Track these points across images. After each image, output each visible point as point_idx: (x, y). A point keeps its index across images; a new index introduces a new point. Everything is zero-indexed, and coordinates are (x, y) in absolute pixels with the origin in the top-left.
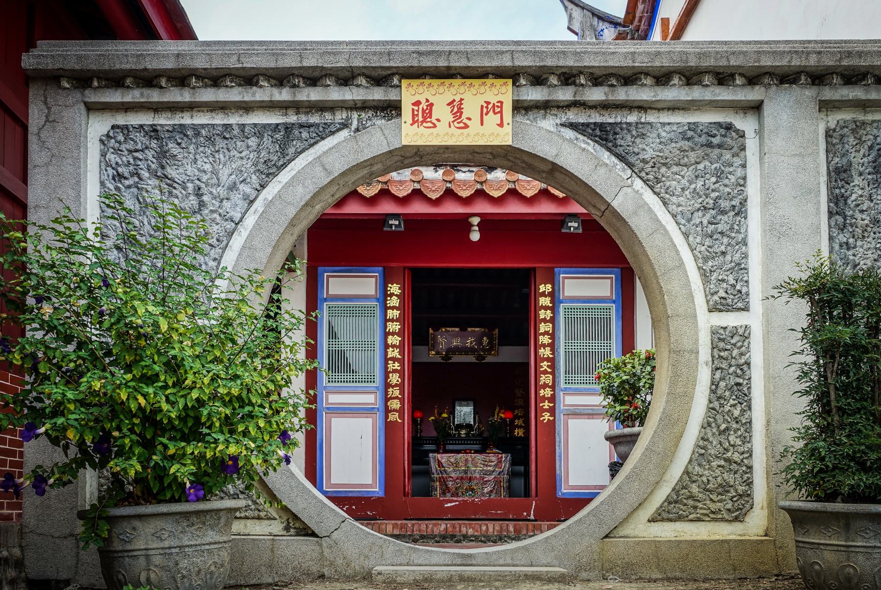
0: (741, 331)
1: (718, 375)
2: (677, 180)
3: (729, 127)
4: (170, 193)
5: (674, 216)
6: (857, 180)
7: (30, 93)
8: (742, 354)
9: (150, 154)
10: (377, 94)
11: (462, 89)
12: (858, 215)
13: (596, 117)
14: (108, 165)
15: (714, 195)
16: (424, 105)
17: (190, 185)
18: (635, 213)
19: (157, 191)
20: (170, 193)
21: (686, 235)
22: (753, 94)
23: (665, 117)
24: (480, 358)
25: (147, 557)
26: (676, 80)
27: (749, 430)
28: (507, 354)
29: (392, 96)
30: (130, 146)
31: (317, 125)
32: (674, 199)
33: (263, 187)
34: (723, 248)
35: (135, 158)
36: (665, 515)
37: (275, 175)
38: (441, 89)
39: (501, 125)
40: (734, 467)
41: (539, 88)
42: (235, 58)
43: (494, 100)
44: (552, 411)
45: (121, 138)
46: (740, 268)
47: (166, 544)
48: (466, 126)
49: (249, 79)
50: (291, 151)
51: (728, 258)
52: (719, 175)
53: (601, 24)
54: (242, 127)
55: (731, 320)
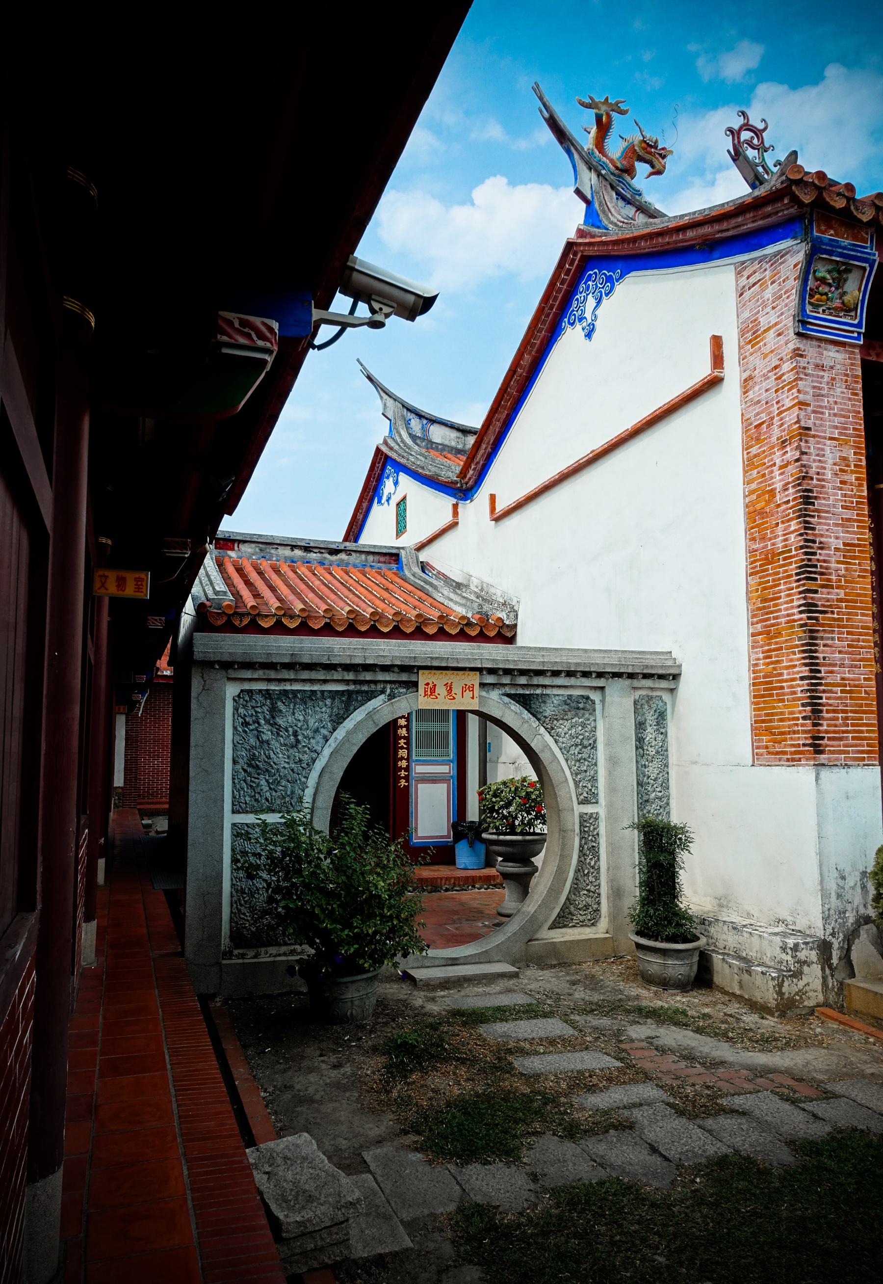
0: (594, 816)
1: (583, 842)
2: (563, 727)
3: (588, 698)
4: (278, 734)
5: (561, 749)
6: (649, 729)
7: (193, 671)
8: (594, 829)
9: (265, 708)
10: (404, 677)
11: (452, 677)
12: (650, 749)
13: (521, 691)
14: (239, 715)
15: (581, 737)
16: (431, 685)
17: (290, 729)
18: (543, 751)
19: (269, 733)
20: (278, 734)
21: (567, 760)
22: (601, 683)
23: (556, 691)
25: (352, 1001)
26: (563, 675)
27: (598, 873)
29: (414, 678)
30: (253, 703)
31: (367, 692)
32: (561, 739)
33: (334, 730)
34: (585, 768)
35: (256, 712)
36: (557, 925)
37: (341, 723)
38: (441, 676)
39: (473, 698)
40: (591, 894)
41: (492, 676)
42: (326, 657)
43: (469, 684)
44: (407, 778)
45: (247, 698)
46: (594, 779)
47: (361, 994)
48: (454, 698)
50: (352, 708)
51: (588, 774)
52: (584, 726)
53: (409, 414)
54: (322, 692)
55: (589, 809)
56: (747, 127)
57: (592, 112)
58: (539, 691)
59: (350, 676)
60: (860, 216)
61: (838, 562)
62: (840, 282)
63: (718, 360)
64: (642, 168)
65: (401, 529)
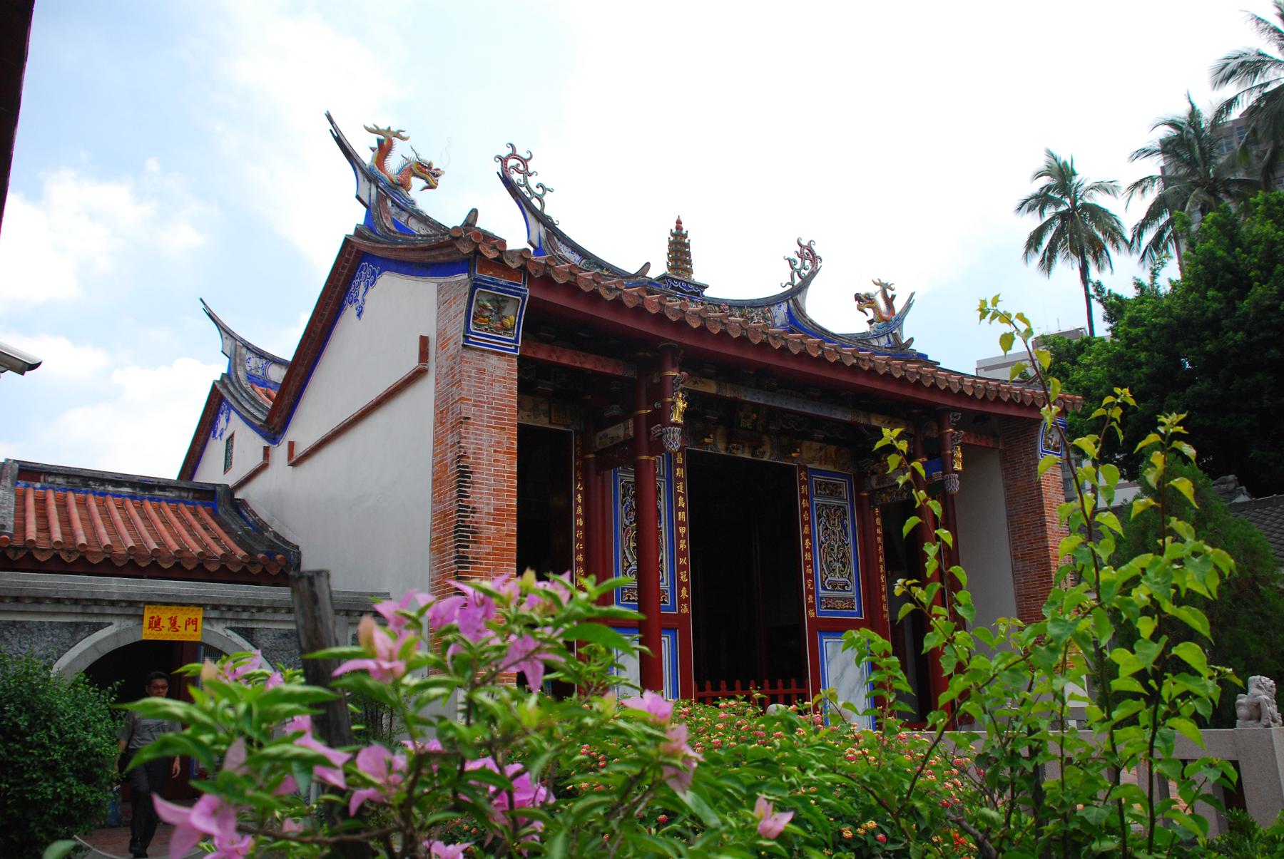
13: (241, 625)
24: (670, 625)
28: (178, 759)
43: (193, 617)
49: (58, 601)
56: (513, 155)
57: (376, 136)
58: (261, 626)
59: (79, 609)
60: (510, 264)
61: (488, 523)
62: (499, 309)
63: (424, 355)
64: (417, 183)
65: (227, 466)
